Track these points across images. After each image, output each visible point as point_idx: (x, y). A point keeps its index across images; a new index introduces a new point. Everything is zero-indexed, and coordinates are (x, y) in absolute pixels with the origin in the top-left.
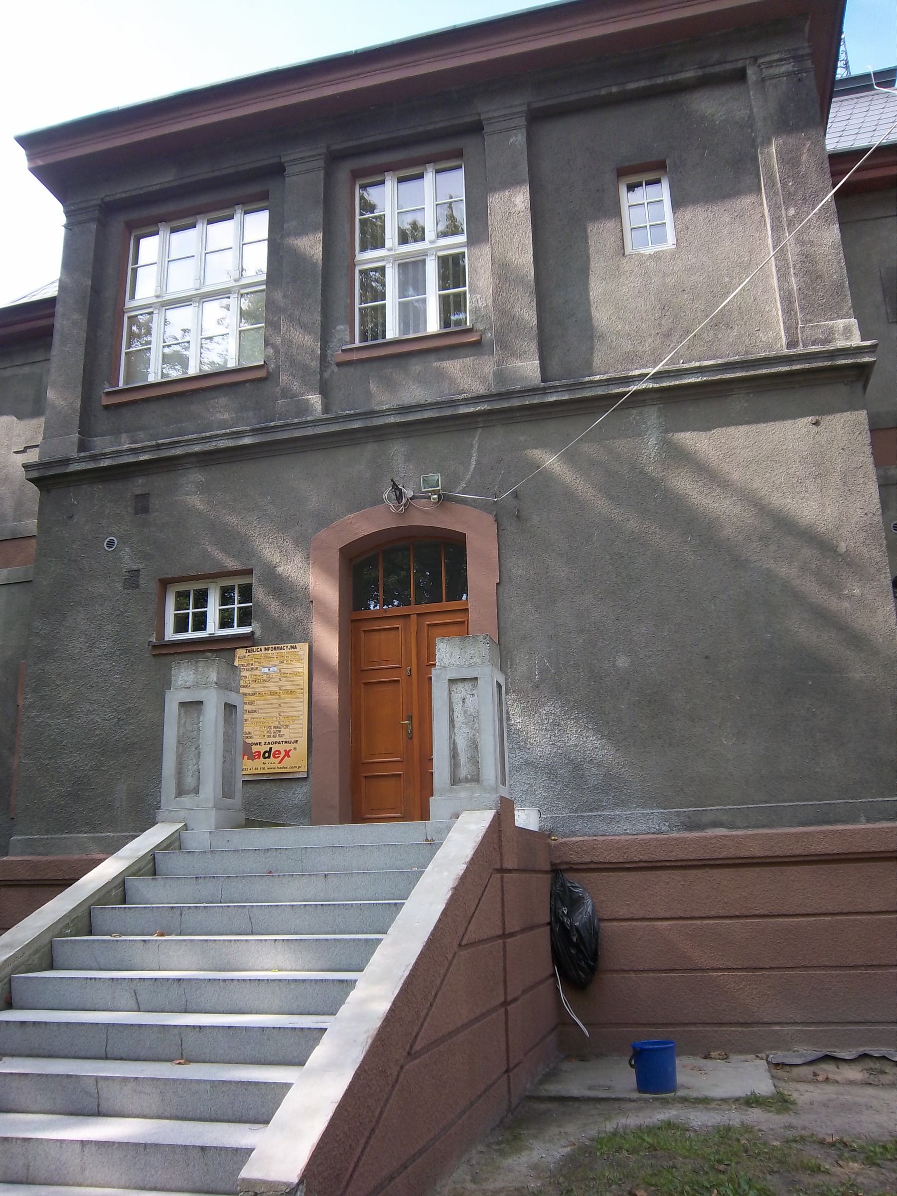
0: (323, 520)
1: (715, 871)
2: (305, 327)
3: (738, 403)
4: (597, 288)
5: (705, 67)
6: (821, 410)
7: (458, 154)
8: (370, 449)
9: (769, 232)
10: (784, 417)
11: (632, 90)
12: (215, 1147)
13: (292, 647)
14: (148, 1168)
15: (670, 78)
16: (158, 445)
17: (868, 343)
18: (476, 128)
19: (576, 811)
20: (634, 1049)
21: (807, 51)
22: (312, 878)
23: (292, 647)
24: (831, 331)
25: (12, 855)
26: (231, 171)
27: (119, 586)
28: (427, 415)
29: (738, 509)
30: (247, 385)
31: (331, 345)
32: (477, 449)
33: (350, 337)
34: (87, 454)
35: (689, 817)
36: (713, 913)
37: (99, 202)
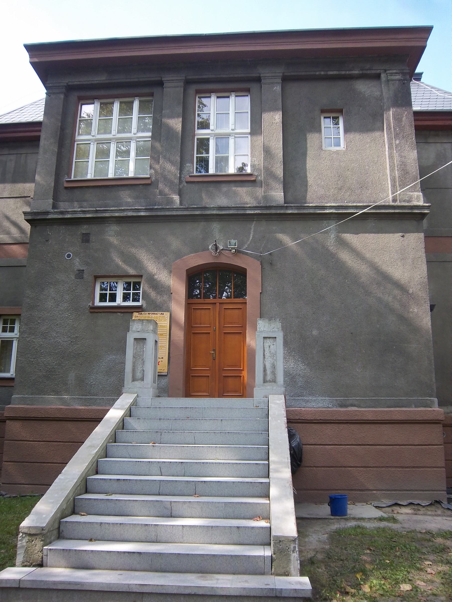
0: (179, 255)
1: (351, 425)
2: (172, 163)
3: (371, 223)
4: (310, 163)
5: (363, 70)
6: (405, 231)
7: (248, 90)
8: (202, 224)
9: (387, 149)
10: (386, 232)
11: (330, 75)
12: (244, 527)
13: (162, 314)
14: (213, 536)
15: (348, 72)
16: (97, 211)
17: (427, 205)
18: (258, 80)
19: (292, 397)
20: (331, 498)
21: (408, 71)
22: (216, 421)
23: (162, 314)
24: (411, 197)
25: (13, 404)
26: (136, 80)
27: (73, 277)
28: (231, 212)
29: (368, 270)
30: (141, 186)
31: (184, 172)
32: (253, 230)
33: (193, 168)
34: (59, 210)
35: (341, 402)
36: (350, 443)
37: (66, 84)
